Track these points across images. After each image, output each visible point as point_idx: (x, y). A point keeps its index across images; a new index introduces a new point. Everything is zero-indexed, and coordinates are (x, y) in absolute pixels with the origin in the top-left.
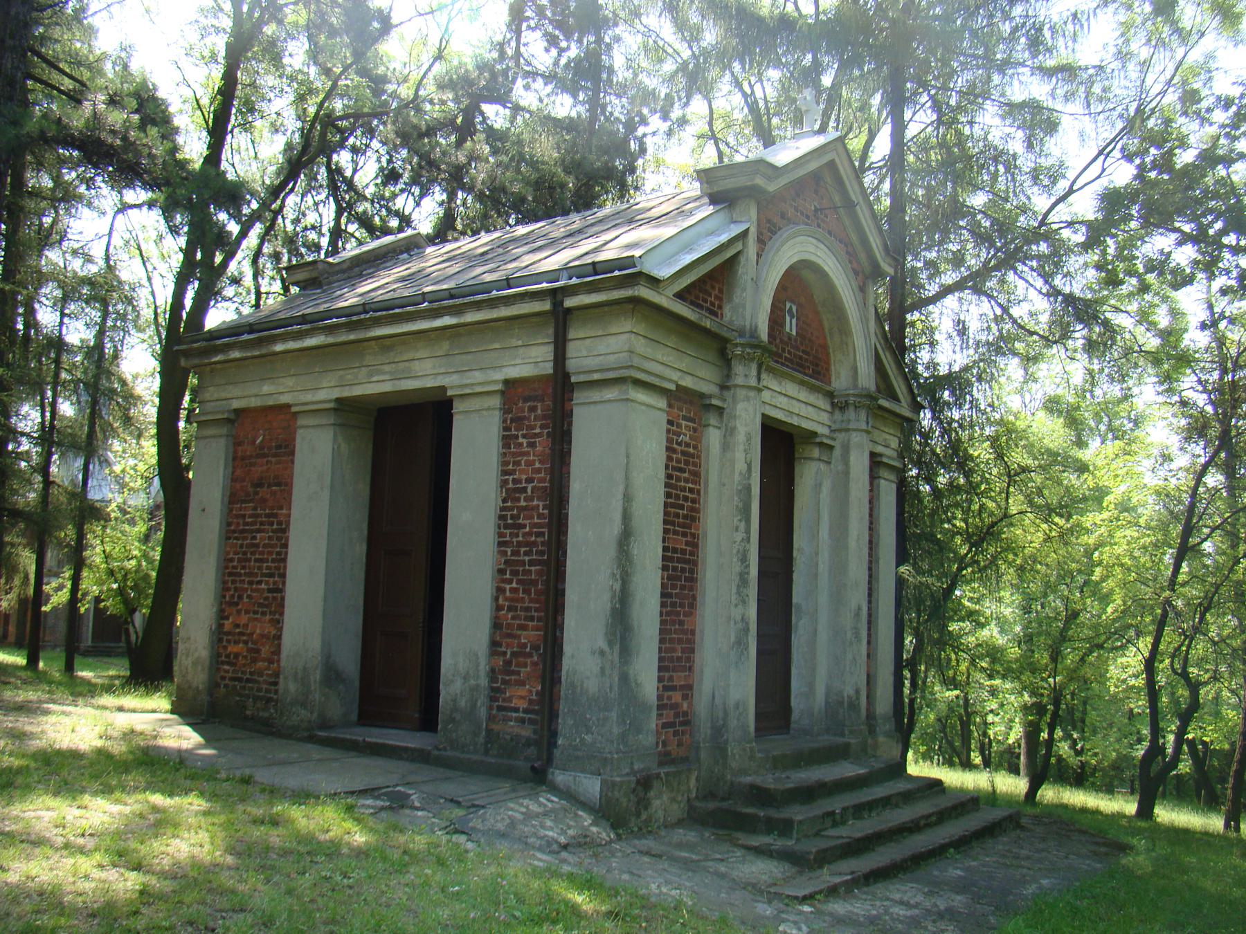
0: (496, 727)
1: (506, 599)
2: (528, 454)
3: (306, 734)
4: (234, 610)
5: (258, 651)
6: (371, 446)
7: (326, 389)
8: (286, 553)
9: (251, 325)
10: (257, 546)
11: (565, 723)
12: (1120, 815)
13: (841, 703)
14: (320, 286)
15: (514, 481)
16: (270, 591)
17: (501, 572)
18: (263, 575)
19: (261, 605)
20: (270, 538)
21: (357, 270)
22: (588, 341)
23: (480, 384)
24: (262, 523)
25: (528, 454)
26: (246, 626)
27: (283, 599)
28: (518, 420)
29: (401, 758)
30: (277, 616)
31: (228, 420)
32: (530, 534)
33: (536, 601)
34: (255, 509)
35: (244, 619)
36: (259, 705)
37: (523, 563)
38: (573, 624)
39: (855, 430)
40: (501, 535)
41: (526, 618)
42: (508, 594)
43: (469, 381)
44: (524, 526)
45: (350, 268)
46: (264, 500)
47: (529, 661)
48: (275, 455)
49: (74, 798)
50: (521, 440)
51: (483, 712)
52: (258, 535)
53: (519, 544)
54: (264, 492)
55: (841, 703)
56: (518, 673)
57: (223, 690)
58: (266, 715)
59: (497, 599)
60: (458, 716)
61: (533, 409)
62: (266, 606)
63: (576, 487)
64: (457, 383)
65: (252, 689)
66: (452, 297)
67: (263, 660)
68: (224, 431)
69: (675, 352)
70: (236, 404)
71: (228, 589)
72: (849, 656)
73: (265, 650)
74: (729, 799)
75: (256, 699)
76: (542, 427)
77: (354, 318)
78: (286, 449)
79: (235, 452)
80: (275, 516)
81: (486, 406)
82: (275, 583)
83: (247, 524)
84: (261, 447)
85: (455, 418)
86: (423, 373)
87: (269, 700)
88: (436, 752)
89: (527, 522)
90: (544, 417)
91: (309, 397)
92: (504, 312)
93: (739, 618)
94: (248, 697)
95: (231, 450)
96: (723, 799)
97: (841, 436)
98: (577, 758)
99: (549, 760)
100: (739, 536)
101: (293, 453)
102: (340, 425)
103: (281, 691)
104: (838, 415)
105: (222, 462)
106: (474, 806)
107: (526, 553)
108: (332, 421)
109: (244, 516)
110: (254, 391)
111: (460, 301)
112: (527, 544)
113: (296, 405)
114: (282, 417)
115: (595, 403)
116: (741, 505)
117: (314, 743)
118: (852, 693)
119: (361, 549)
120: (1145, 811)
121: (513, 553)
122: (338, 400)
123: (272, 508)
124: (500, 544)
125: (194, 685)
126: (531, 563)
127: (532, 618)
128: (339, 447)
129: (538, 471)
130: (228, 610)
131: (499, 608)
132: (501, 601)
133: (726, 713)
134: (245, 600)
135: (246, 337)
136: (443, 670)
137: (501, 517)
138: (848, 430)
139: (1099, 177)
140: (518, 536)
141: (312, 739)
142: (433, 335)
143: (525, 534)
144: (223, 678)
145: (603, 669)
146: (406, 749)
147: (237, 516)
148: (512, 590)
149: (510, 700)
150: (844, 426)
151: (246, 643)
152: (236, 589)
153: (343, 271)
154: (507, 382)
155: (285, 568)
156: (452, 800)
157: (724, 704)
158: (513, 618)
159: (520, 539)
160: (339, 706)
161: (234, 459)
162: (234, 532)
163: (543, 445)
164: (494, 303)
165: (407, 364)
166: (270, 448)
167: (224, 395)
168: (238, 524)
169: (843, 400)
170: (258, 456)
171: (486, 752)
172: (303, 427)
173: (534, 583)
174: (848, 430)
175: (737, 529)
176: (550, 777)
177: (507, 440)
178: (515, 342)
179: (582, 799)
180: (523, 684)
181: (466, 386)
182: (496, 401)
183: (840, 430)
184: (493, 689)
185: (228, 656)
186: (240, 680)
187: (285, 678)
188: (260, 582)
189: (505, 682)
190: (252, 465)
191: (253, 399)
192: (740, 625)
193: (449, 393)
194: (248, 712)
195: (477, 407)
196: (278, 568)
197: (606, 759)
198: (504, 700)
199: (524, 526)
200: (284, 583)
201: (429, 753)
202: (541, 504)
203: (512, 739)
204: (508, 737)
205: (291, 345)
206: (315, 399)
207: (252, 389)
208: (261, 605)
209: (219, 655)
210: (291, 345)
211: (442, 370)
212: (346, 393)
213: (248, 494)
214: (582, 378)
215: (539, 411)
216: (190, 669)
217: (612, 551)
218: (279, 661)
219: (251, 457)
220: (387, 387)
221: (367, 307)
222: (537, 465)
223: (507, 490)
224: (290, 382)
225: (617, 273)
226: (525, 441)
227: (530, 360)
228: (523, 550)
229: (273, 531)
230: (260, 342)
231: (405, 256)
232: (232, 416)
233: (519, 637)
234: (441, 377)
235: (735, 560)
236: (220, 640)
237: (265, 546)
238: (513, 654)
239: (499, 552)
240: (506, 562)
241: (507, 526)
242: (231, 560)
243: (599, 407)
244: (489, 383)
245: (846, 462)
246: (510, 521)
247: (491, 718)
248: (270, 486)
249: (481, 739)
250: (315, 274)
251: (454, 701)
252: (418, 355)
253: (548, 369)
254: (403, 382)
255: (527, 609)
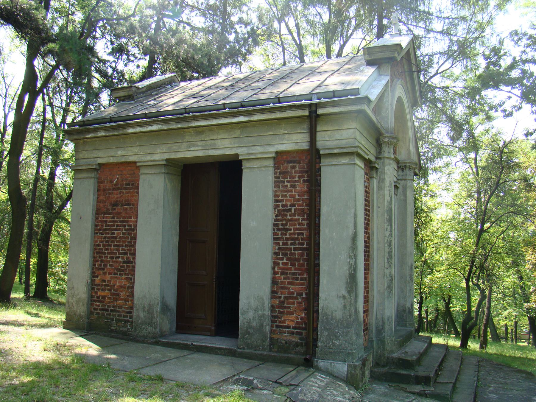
0: (276, 337)
1: (280, 268)
2: (291, 191)
3: (154, 340)
4: (101, 272)
5: (118, 295)
6: (180, 185)
7: (161, 154)
8: (135, 242)
9: (110, 118)
10: (116, 238)
11: (322, 335)
12: (454, 347)
13: (404, 311)
14: (133, 99)
15: (283, 206)
16: (124, 262)
17: (276, 254)
18: (120, 254)
19: (119, 270)
20: (123, 234)
21: (149, 92)
22: (329, 133)
23: (260, 153)
24: (118, 226)
25: (291, 191)
26: (110, 281)
27: (134, 267)
28: (284, 173)
29: (216, 354)
30: (130, 276)
31: (95, 169)
32: (294, 234)
33: (299, 270)
34: (113, 217)
35: (108, 277)
36: (119, 323)
37: (290, 249)
38: (325, 282)
39: (409, 180)
40: (275, 234)
41: (293, 279)
42: (281, 265)
43: (253, 152)
44: (290, 230)
45: (146, 91)
46: (119, 213)
47: (295, 301)
48: (125, 189)
49: (22, 382)
50: (286, 184)
51: (268, 329)
52: (116, 232)
53: (287, 239)
54: (119, 209)
55: (404, 311)
56: (289, 308)
57: (96, 315)
58: (125, 329)
59: (274, 268)
60: (251, 331)
61: (294, 167)
62: (123, 271)
63: (324, 209)
64: (246, 152)
65: (115, 315)
66: (243, 106)
67: (122, 300)
68: (93, 175)
69: (366, 139)
70: (100, 161)
71: (97, 261)
72: (408, 288)
73: (123, 294)
74: (387, 366)
75: (118, 321)
76: (299, 177)
77: (182, 116)
78: (133, 186)
79: (99, 186)
80: (127, 222)
81: (264, 165)
82: (128, 258)
83: (109, 226)
84: (116, 185)
85: (243, 171)
86: (224, 147)
87: (126, 322)
88: (238, 350)
89: (292, 227)
90: (301, 172)
91: (148, 158)
92: (278, 115)
93: (388, 275)
94: (112, 319)
95: (96, 185)
96: (384, 366)
97: (402, 183)
98: (331, 353)
99: (314, 354)
100: (387, 233)
101: (138, 188)
102: (167, 173)
103: (134, 317)
104: (400, 172)
105: (92, 192)
106: (291, 385)
107: (291, 244)
108: (163, 171)
109: (106, 222)
110: (113, 154)
111: (251, 108)
112: (292, 239)
113: (139, 162)
114: (133, 167)
115: (335, 165)
116: (388, 218)
117: (159, 345)
118: (410, 306)
119: (176, 239)
120: (464, 344)
121: (283, 244)
122: (167, 160)
123: (125, 217)
124: (275, 239)
125: (78, 313)
126: (295, 249)
127: (297, 279)
128: (167, 185)
129: (298, 200)
130: (97, 272)
131: (275, 273)
132: (276, 270)
133: (383, 323)
134: (108, 267)
135: (108, 124)
136: (241, 306)
137: (275, 225)
138: (406, 180)
139: (450, 67)
140: (286, 235)
141: (157, 343)
142: (230, 126)
143: (290, 234)
144: (95, 309)
145: (345, 306)
146: (220, 349)
147: (102, 222)
148: (283, 264)
149: (284, 322)
150: (404, 177)
151: (110, 290)
152: (102, 261)
153: (143, 92)
154: (277, 153)
155: (135, 250)
156: (276, 382)
157: (382, 318)
158: (284, 278)
159: (288, 236)
160: (167, 323)
161: (98, 190)
162: (100, 230)
163: (301, 186)
164: (281, 109)
165: (213, 142)
166: (122, 185)
167: (92, 156)
168: (102, 226)
169: (404, 165)
170: (114, 189)
171: (270, 350)
172: (143, 174)
173: (298, 260)
174: (406, 180)
175: (387, 230)
176: (315, 363)
177: (277, 184)
178: (282, 132)
179: (336, 375)
180: (292, 313)
181: (252, 154)
182: (271, 163)
183: (402, 180)
184: (272, 316)
185: (98, 297)
186: (107, 310)
187: (137, 310)
188: (118, 258)
189: (280, 312)
190: (110, 194)
191: (111, 158)
192: (389, 278)
193: (241, 158)
194: (112, 328)
195: (258, 165)
196: (130, 250)
197: (349, 353)
198: (280, 322)
199: (290, 230)
200: (134, 258)
201: (235, 351)
202: (300, 218)
203: (286, 343)
204: (284, 342)
205: (139, 129)
206: (152, 159)
207: (112, 153)
208: (119, 270)
209: (92, 297)
210: (139, 129)
211: (236, 145)
212: (173, 156)
213: (108, 209)
214: (327, 152)
215: (297, 169)
216: (74, 304)
217: (349, 244)
218: (132, 300)
219: (110, 189)
220: (200, 154)
221: (187, 110)
222: (297, 197)
223: (279, 211)
224: (136, 150)
225: (349, 97)
226: (289, 184)
227: (295, 141)
228: (289, 242)
229: (125, 230)
230: (118, 127)
231: (169, 86)
232: (97, 167)
233: (289, 289)
234: (235, 149)
235: (386, 245)
236: (93, 289)
237: (120, 238)
238: (285, 297)
239: (274, 243)
240: (279, 249)
241: (279, 230)
242: (99, 245)
243: (337, 167)
244: (266, 153)
245: (405, 196)
246: (280, 227)
247: (272, 332)
248: (122, 205)
249: (267, 343)
250: (130, 93)
251: (249, 323)
252: (220, 137)
253: (305, 146)
254: (210, 151)
255: (294, 274)
